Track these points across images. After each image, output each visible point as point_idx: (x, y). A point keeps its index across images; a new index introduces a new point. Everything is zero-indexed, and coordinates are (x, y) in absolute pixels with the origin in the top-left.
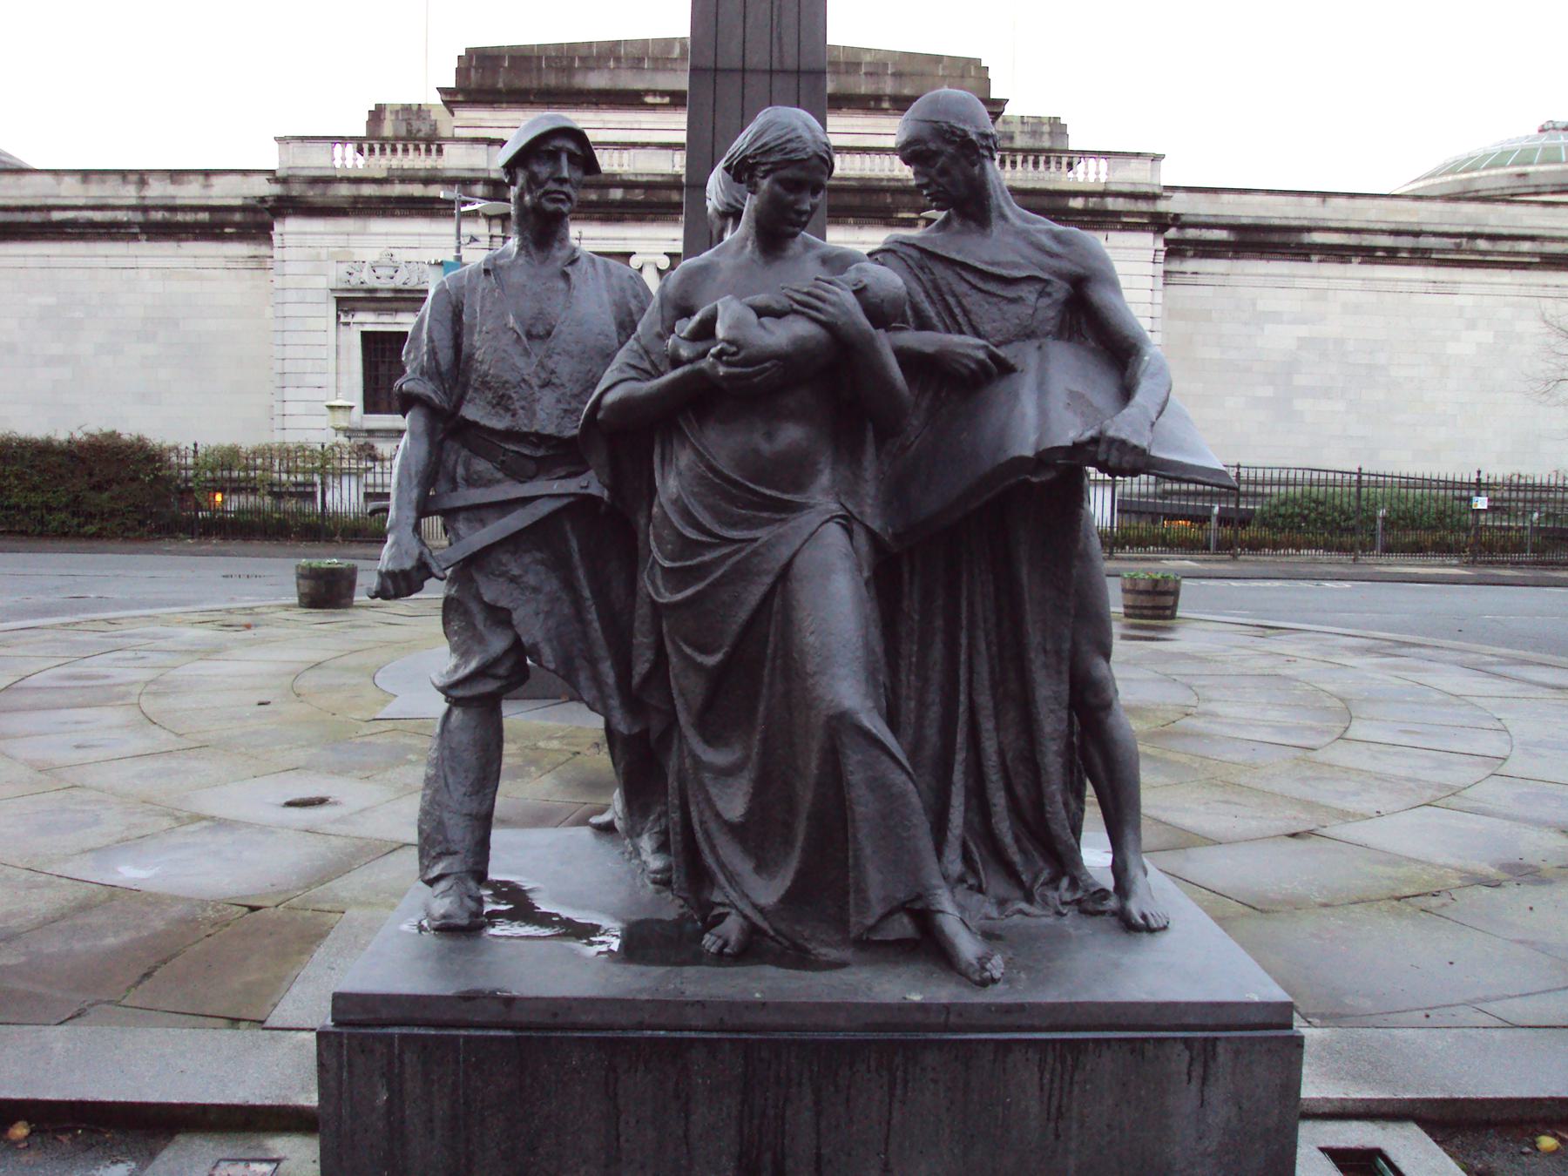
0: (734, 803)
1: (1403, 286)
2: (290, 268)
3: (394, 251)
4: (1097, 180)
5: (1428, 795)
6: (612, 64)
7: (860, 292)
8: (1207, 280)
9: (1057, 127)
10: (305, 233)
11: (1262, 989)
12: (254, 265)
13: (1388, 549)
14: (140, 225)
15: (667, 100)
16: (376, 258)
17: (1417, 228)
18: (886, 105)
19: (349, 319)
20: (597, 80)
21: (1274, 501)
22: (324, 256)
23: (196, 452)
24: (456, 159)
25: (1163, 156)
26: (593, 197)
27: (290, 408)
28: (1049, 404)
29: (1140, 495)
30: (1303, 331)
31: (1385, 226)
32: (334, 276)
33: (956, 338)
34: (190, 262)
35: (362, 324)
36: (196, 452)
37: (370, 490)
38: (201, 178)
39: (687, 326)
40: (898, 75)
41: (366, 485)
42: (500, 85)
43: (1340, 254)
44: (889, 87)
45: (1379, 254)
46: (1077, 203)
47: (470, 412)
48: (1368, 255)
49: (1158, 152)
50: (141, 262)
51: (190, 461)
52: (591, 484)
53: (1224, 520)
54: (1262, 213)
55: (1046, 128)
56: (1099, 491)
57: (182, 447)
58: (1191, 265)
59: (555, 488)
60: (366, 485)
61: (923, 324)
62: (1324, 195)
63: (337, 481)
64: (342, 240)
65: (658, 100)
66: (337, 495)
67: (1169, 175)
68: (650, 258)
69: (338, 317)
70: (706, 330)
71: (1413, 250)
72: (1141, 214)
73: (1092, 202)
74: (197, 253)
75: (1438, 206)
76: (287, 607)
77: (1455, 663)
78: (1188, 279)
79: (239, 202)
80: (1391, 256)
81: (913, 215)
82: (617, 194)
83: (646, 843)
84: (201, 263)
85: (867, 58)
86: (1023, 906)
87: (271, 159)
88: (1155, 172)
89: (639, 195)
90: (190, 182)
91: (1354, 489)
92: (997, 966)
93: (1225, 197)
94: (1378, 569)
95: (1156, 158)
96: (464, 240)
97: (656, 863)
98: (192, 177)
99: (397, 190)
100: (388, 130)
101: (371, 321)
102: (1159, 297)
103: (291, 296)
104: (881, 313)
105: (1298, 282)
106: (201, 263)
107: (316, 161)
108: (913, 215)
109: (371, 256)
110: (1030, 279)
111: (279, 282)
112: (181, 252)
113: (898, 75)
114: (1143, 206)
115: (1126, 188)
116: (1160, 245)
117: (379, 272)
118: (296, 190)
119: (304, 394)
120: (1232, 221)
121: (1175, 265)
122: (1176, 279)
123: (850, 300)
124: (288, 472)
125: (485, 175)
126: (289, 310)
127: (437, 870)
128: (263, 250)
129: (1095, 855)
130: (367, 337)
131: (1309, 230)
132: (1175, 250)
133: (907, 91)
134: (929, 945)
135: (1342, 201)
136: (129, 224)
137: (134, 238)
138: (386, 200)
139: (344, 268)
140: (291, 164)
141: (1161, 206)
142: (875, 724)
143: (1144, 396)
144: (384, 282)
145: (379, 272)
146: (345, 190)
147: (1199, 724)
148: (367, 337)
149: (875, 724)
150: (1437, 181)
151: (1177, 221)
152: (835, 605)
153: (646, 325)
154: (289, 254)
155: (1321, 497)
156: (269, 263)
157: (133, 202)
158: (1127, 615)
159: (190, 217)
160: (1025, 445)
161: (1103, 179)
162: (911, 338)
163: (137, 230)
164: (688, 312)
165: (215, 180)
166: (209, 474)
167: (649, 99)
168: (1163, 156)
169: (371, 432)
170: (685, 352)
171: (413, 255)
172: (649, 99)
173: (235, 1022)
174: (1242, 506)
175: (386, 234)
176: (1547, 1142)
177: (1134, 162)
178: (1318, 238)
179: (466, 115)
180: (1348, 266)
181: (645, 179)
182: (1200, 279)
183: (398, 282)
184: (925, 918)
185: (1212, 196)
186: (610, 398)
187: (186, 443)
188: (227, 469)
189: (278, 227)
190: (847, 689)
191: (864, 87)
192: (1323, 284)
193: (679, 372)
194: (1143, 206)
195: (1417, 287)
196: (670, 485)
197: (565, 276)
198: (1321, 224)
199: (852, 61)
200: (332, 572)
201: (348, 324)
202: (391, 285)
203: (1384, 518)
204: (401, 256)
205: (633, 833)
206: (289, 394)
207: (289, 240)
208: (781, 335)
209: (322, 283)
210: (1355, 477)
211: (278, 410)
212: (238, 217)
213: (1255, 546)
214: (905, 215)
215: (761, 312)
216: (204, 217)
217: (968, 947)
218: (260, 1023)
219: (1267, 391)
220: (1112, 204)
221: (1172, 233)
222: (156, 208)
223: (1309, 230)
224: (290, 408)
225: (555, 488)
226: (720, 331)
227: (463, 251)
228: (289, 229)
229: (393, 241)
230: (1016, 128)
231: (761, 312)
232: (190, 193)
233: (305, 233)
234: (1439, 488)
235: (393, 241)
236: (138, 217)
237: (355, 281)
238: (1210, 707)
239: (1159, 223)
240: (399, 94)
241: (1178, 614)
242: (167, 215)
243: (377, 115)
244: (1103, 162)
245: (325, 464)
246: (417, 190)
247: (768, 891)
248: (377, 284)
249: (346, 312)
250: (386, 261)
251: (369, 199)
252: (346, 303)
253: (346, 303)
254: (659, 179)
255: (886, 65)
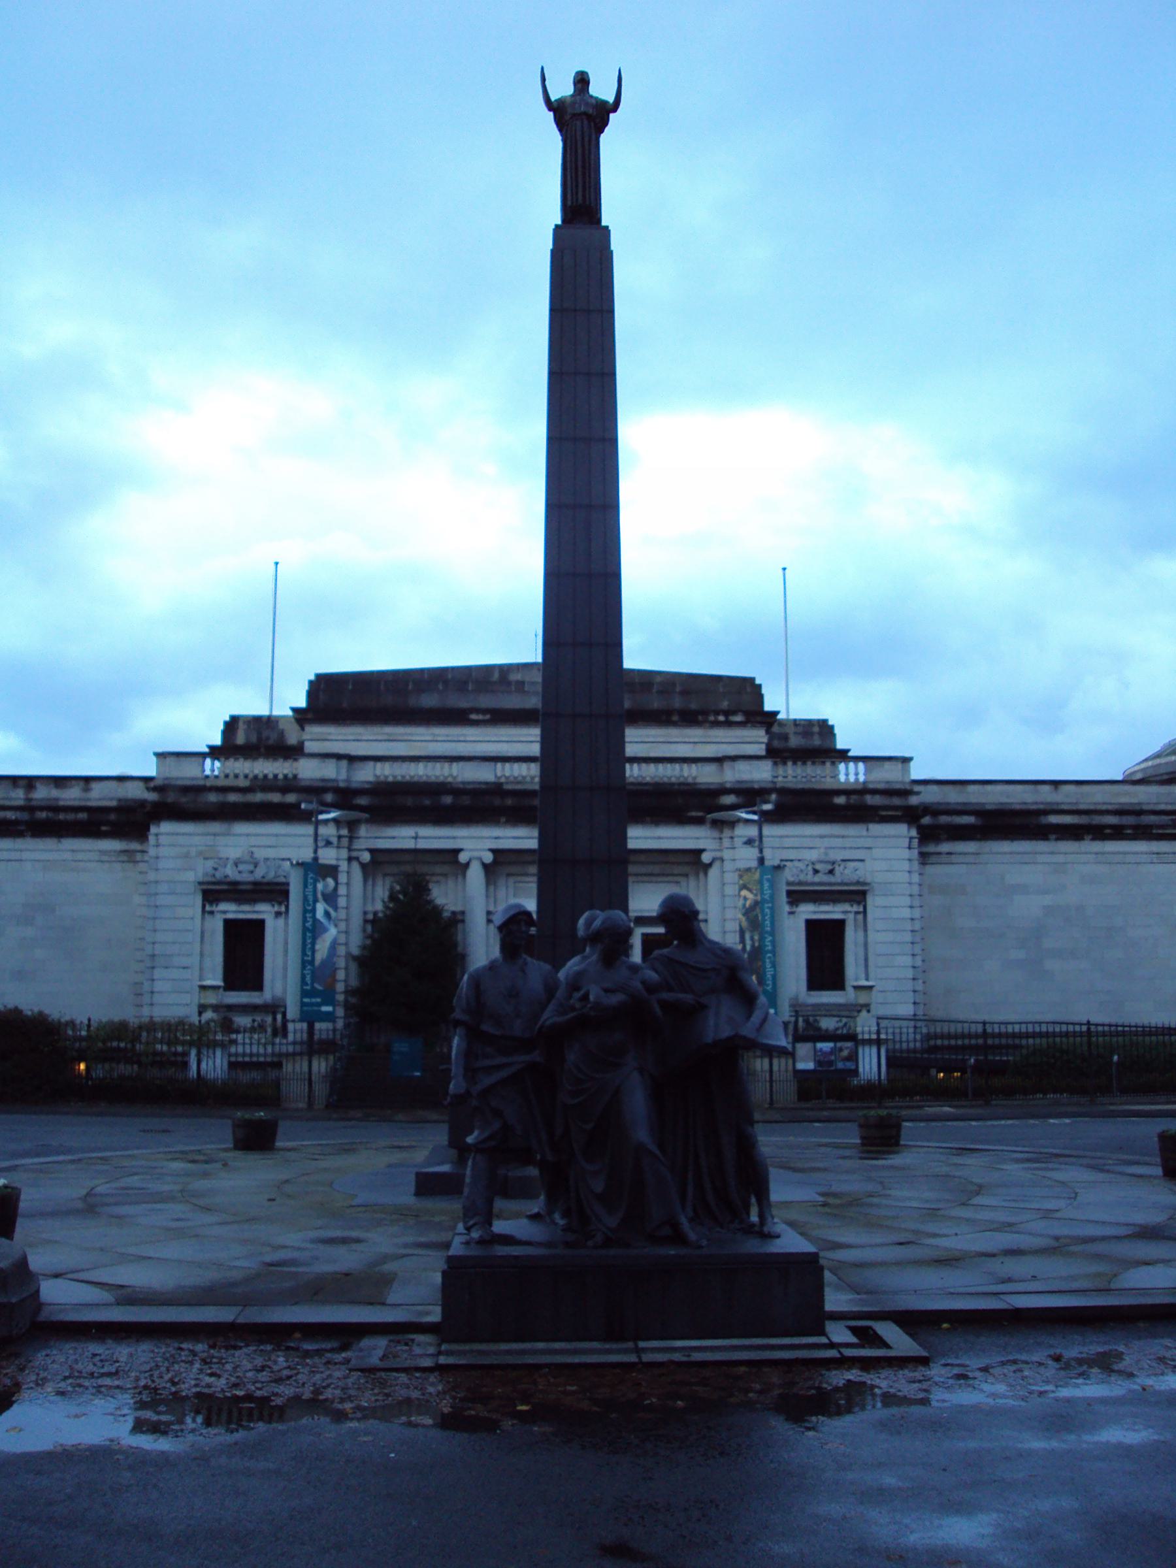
0: (598, 1186)
1: (1129, 858)
2: (162, 864)
3: (253, 849)
4: (857, 780)
5: (995, 1226)
6: (441, 687)
7: (643, 982)
8: (961, 859)
9: (825, 729)
10: (177, 834)
11: (810, 1248)
12: (125, 858)
13: (1124, 1091)
14: (26, 823)
15: (488, 717)
16: (238, 855)
17: (1138, 808)
18: (675, 718)
19: (214, 908)
20: (429, 701)
21: (1024, 1051)
22: (193, 854)
23: (89, 1026)
24: (308, 770)
25: (910, 759)
26: (427, 802)
27: (158, 986)
28: (720, 1021)
29: (908, 1051)
30: (1047, 900)
31: (1110, 807)
32: (201, 870)
33: (681, 996)
34: (67, 856)
35: (225, 912)
36: (89, 1026)
37: (233, 1059)
38: (82, 783)
39: (577, 995)
40: (685, 693)
41: (230, 1055)
42: (345, 705)
43: (1073, 833)
44: (677, 703)
45: (1108, 831)
46: (840, 800)
47: (485, 1027)
48: (1099, 833)
49: (907, 755)
50: (26, 855)
51: (84, 1033)
52: (536, 1056)
53: (978, 1069)
54: (1005, 800)
55: (816, 729)
56: (867, 1049)
57: (78, 1022)
58: (945, 847)
59: (523, 1058)
60: (230, 1055)
61: (670, 990)
62: (1056, 784)
63: (211, 1051)
64: (209, 840)
65: (481, 717)
66: (211, 1063)
67: (917, 772)
68: (476, 854)
69: (204, 906)
70: (585, 997)
71: (1135, 827)
72: (895, 808)
73: (854, 798)
74: (75, 847)
75: (1154, 789)
76: (226, 1150)
77: (1081, 1165)
78: (944, 858)
79: (114, 803)
80: (1117, 833)
81: (700, 814)
82: (448, 800)
83: (557, 1216)
84: (80, 856)
85: (658, 679)
86: (718, 1229)
87: (149, 768)
88: (907, 771)
89: (466, 801)
90: (71, 787)
91: (1085, 1039)
92: (704, 1243)
93: (971, 788)
94: (1112, 1108)
95: (906, 760)
96: (320, 844)
97: (561, 1222)
98: (74, 782)
99: (259, 797)
100: (240, 739)
101: (231, 910)
102: (916, 878)
103: (163, 888)
104: (650, 988)
105: (1040, 858)
106: (80, 856)
107: (187, 773)
108: (700, 814)
109: (234, 853)
110: (714, 969)
111: (152, 876)
112: (61, 846)
113: (685, 693)
114: (896, 801)
115: (881, 786)
116: (914, 833)
117: (241, 867)
118: (171, 798)
119: (175, 974)
120: (978, 808)
121: (931, 848)
122: (933, 859)
123: (640, 986)
124: (169, 1044)
125: (335, 784)
126: (161, 900)
127: (471, 1223)
128: (135, 846)
129: (754, 1218)
130: (228, 924)
131: (1046, 812)
132: (928, 835)
133: (694, 706)
134: (678, 1238)
135: (1072, 788)
136: (16, 822)
137: (19, 834)
138: (248, 806)
139: (210, 864)
140: (167, 775)
141: (914, 800)
142: (653, 1148)
143: (756, 1017)
144: (243, 875)
145: (241, 867)
146: (213, 798)
147: (875, 1200)
148: (228, 924)
149: (653, 1148)
150: (1163, 761)
151: (927, 809)
152: (637, 1102)
153: (560, 993)
154: (163, 851)
155: (1064, 1047)
156: (139, 857)
157: (21, 803)
158: (863, 1144)
159: (71, 817)
160: (710, 1037)
161: (862, 778)
162: (665, 995)
163: (22, 828)
164: (577, 989)
165: (94, 785)
166: (100, 1044)
167: (473, 717)
168: (910, 759)
169: (231, 1008)
170: (578, 1005)
171: (271, 853)
172: (473, 717)
173: (371, 1304)
174: (990, 1057)
175: (248, 835)
176: (945, 1325)
177: (887, 765)
178: (1054, 819)
179: (314, 730)
180: (1082, 842)
181: (471, 786)
182: (954, 858)
183: (259, 874)
184: (675, 1226)
185: (959, 787)
186: (548, 1023)
187: (81, 1018)
188: (116, 1041)
189: (153, 829)
190: (642, 1135)
191: (656, 704)
192: (1060, 858)
193: (574, 1014)
194: (896, 801)
195: (1144, 858)
196: (571, 1057)
197: (523, 971)
198: (1055, 807)
199: (646, 680)
200: (261, 1123)
201: (212, 913)
202: (250, 878)
203: (1118, 1063)
204: (260, 854)
205: (550, 1213)
206: (158, 973)
207: (163, 840)
208: (615, 999)
209: (190, 876)
210: (1084, 1028)
211: (147, 986)
212: (113, 817)
213: (1009, 1092)
214: (694, 814)
215: (607, 991)
216: (83, 816)
217: (692, 1236)
218: (384, 1304)
219: (1021, 954)
220: (870, 800)
221: (926, 820)
222: (42, 809)
223: (1046, 812)
224: (158, 986)
225: (523, 1058)
226: (592, 998)
227: (321, 852)
228: (165, 831)
229: (253, 841)
230: (791, 730)
231: (607, 991)
232: (72, 796)
233: (177, 834)
234: (1163, 1035)
235: (253, 841)
236: (25, 816)
237: (219, 875)
238: (889, 1192)
239: (910, 815)
240: (254, 706)
241: (902, 1142)
242: (51, 815)
243: (232, 725)
244: (861, 765)
245: (201, 1038)
246: (275, 798)
247: (612, 1222)
248: (238, 878)
249: (211, 903)
250: (247, 858)
251: (235, 805)
252: (213, 893)
253: (213, 893)
254: (483, 787)
255: (674, 684)
